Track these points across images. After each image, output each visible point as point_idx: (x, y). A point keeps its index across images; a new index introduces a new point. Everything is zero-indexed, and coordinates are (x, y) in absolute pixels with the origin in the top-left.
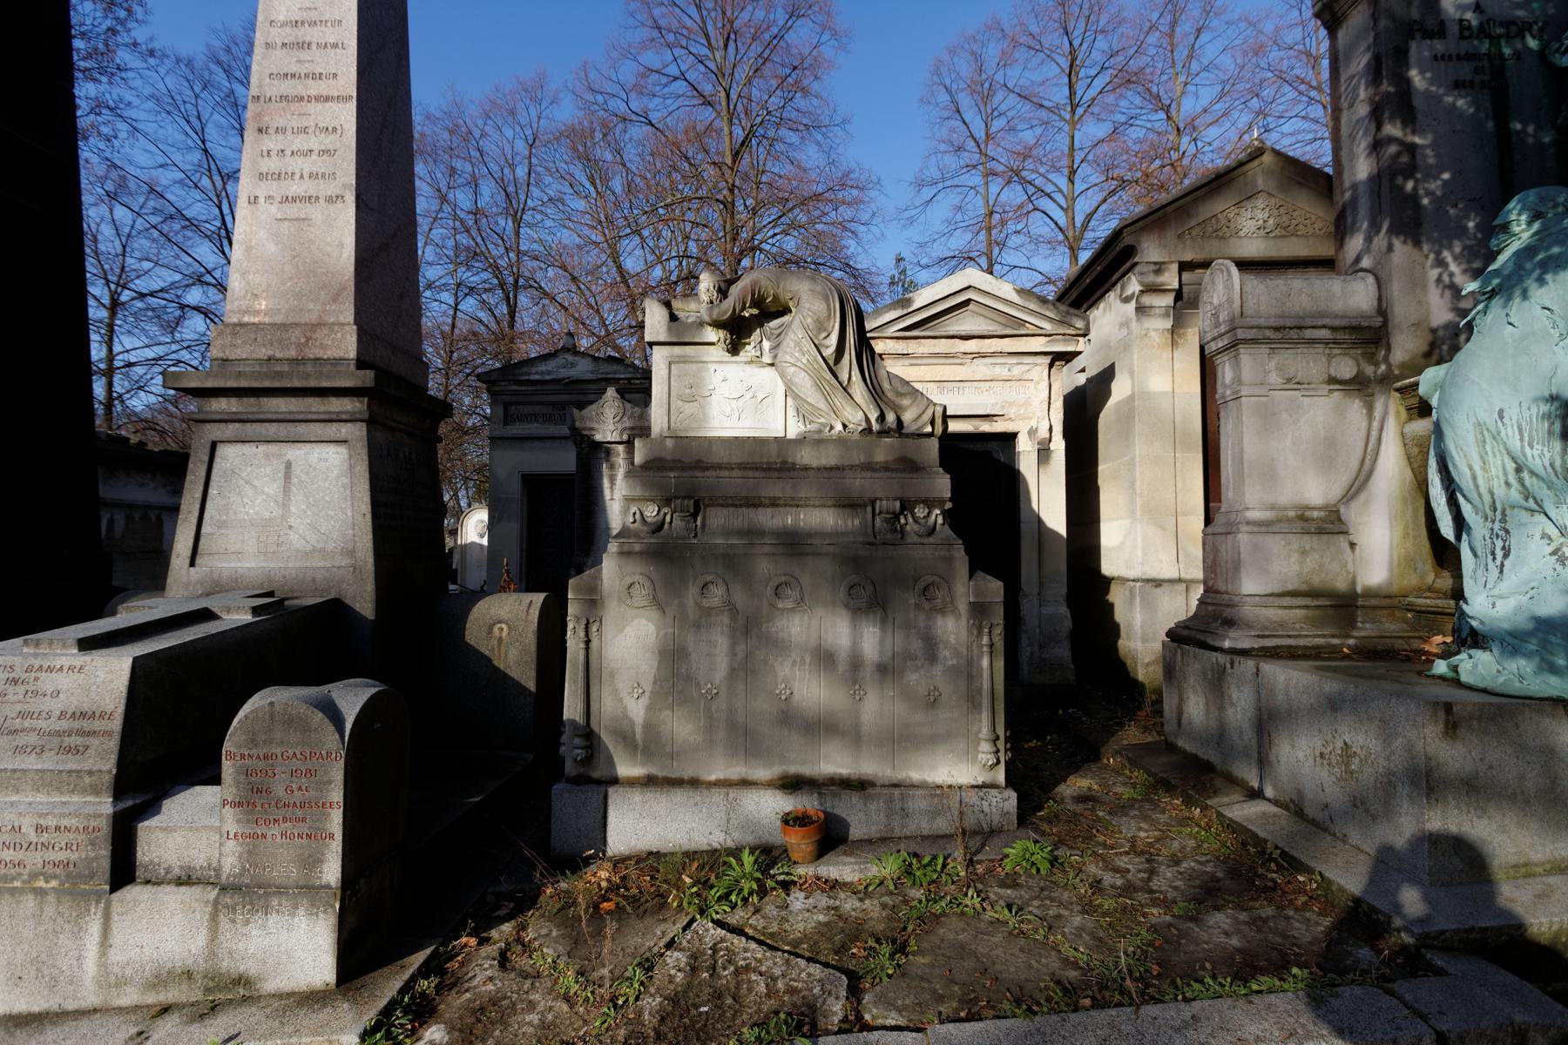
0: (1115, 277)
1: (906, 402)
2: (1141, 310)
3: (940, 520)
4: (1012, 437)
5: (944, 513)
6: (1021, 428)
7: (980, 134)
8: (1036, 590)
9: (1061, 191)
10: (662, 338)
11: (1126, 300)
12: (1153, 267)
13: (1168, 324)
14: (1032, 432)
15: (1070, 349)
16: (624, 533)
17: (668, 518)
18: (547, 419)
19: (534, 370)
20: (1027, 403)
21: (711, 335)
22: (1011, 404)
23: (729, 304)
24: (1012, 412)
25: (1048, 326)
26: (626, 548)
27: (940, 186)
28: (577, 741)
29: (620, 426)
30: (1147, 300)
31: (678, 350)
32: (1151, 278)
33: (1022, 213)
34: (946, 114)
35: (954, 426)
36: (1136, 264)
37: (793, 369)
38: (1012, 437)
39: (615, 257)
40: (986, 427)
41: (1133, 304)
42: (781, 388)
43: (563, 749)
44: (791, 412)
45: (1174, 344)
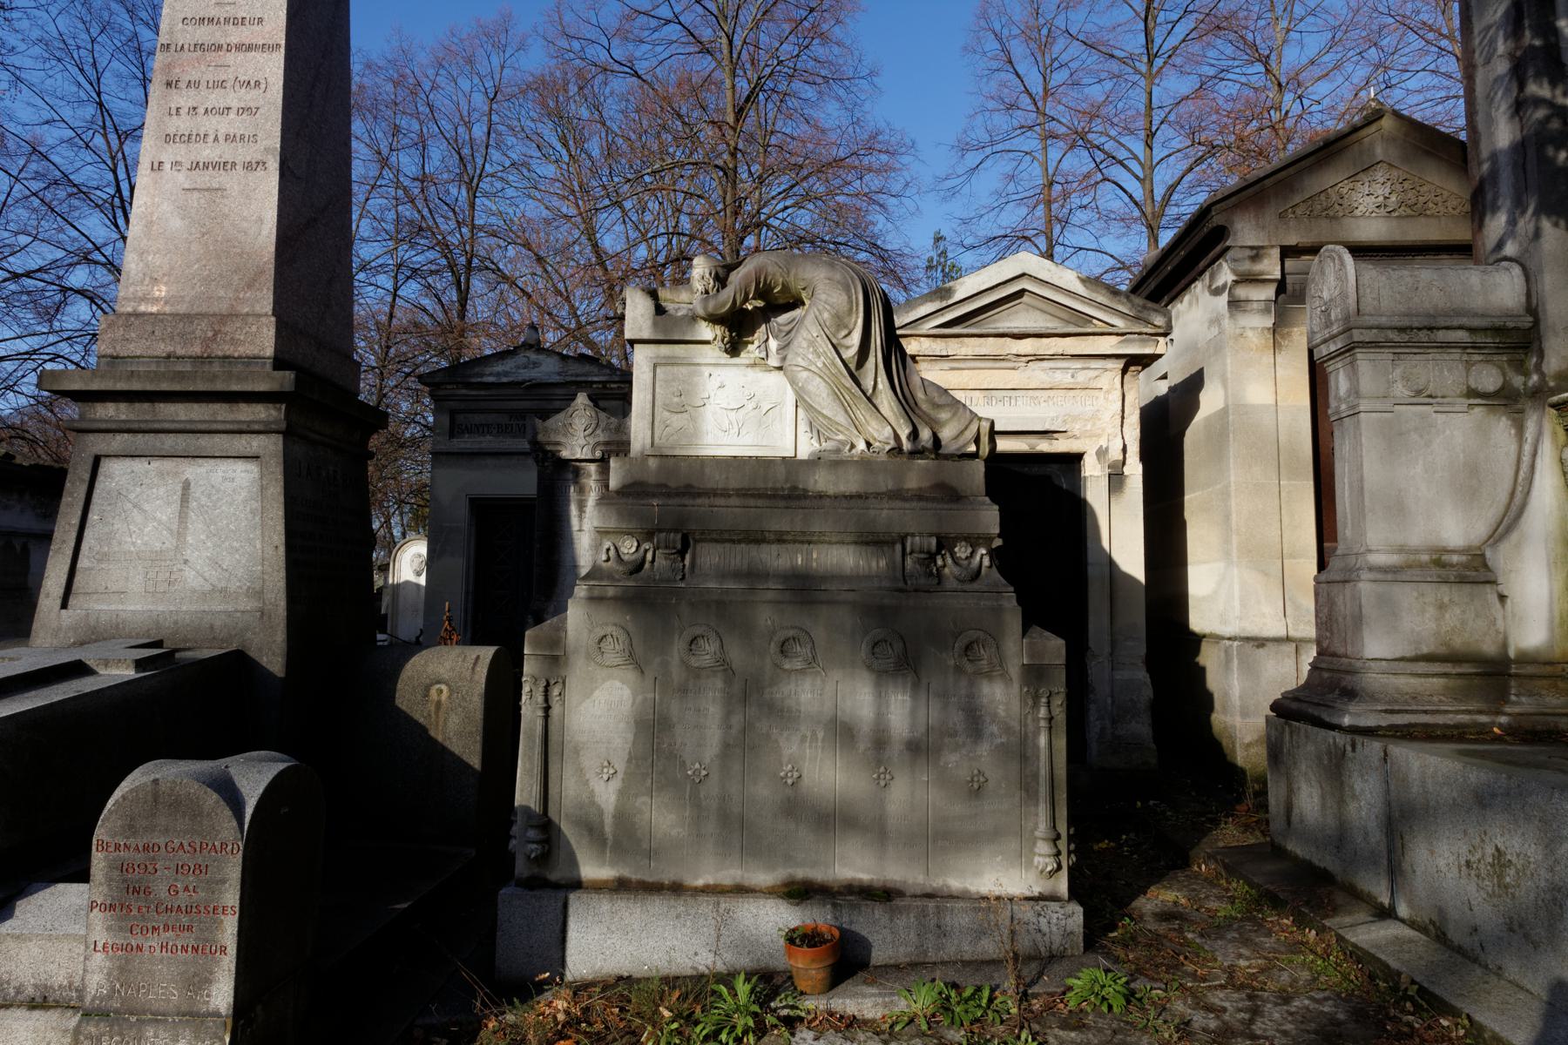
0: (1202, 264)
1: (944, 415)
2: (1235, 304)
3: (986, 562)
4: (1075, 459)
5: (992, 553)
6: (1089, 448)
7: (1037, 88)
8: (1107, 650)
9: (1136, 157)
10: (646, 335)
11: (1217, 292)
12: (1248, 253)
13: (1269, 322)
14: (1102, 453)
15: (1148, 351)
16: (595, 573)
17: (649, 556)
18: (502, 430)
19: (488, 370)
20: (1095, 417)
21: (706, 331)
22: (1075, 419)
23: (727, 294)
24: (1076, 428)
25: (1120, 323)
26: (596, 593)
27: (988, 150)
28: (532, 834)
29: (592, 441)
30: (1242, 292)
31: (665, 350)
32: (1246, 266)
33: (1088, 183)
34: (995, 65)
35: (1003, 445)
36: (1228, 248)
37: (805, 374)
38: (1075, 459)
39: (591, 233)
40: (1044, 446)
41: (1225, 297)
42: (791, 397)
43: (513, 842)
44: (803, 427)
45: (1276, 346)
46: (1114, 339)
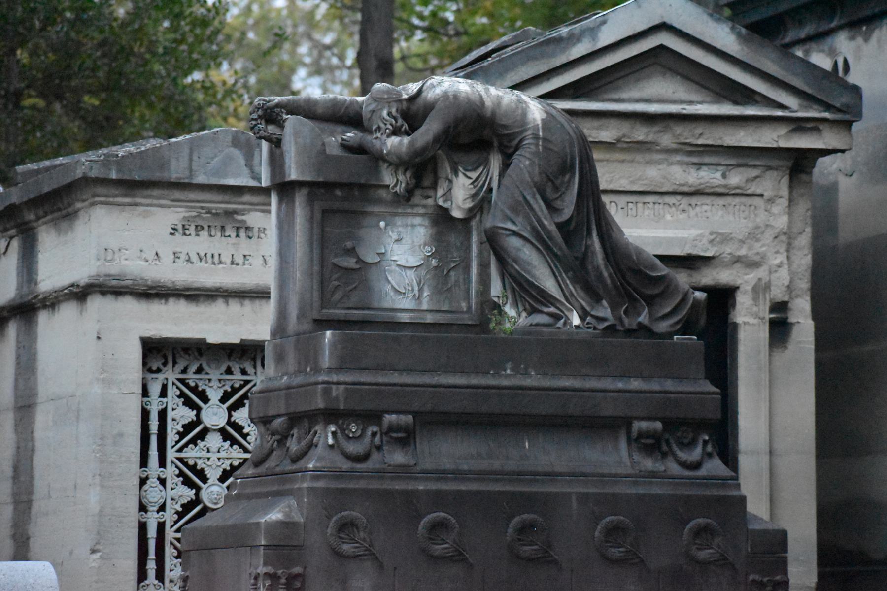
6: (744, 280)
46: (783, 130)
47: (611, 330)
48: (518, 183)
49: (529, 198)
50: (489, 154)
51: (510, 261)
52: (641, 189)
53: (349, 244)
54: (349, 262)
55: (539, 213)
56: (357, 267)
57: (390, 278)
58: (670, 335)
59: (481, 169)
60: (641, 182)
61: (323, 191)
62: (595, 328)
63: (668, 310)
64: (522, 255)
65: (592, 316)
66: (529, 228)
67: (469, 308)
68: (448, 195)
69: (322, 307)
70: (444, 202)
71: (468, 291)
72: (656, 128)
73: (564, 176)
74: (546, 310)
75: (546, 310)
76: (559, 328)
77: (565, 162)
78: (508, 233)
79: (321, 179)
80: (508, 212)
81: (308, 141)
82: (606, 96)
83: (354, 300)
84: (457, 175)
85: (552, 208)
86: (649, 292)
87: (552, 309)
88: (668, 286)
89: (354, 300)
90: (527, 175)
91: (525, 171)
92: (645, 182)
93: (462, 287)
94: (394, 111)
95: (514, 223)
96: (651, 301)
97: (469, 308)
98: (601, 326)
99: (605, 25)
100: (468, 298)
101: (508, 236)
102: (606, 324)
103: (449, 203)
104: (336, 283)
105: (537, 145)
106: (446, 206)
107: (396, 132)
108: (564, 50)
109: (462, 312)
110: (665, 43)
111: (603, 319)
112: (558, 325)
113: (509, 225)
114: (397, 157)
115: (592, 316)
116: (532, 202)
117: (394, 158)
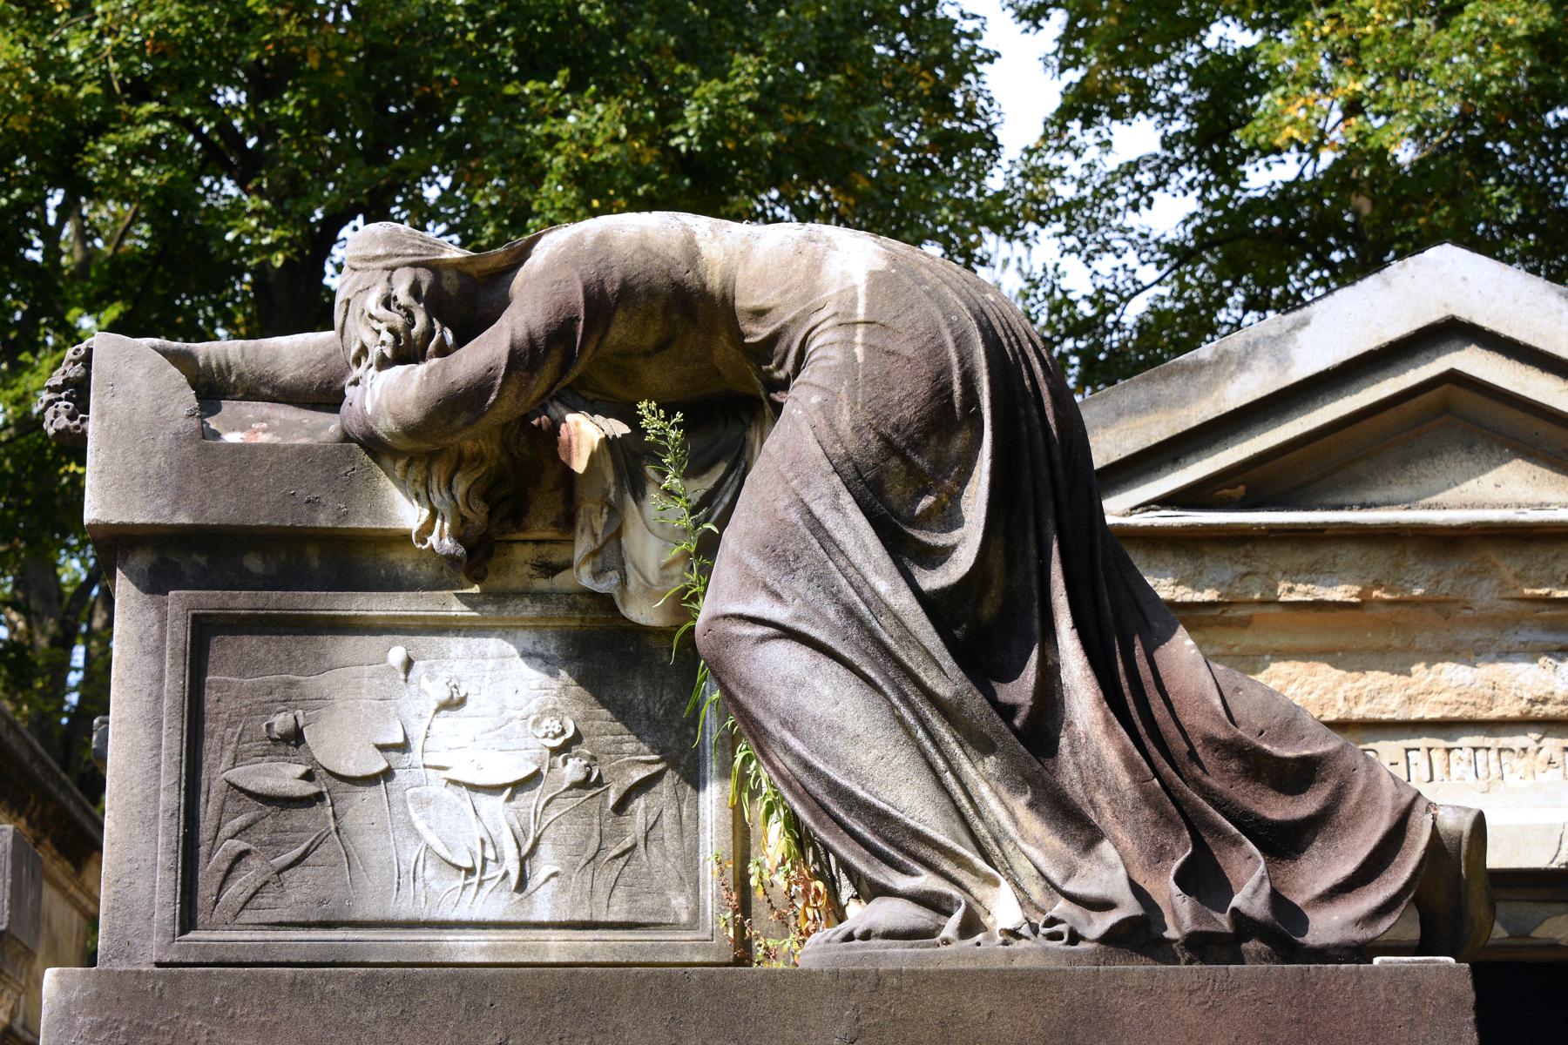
47: (1138, 936)
48: (783, 468)
49: (819, 509)
50: (747, 427)
51: (772, 725)
52: (1436, 714)
53: (281, 722)
54: (285, 777)
55: (857, 558)
56: (310, 789)
57: (420, 825)
58: (1361, 952)
59: (720, 470)
60: (1435, 698)
61: (202, 560)
62: (1075, 938)
63: (1345, 867)
64: (805, 700)
65: (1071, 897)
66: (831, 612)
67: (696, 914)
68: (611, 553)
69: (187, 920)
70: (597, 575)
71: (691, 858)
72: (1456, 566)
73: (946, 439)
74: (902, 883)
75: (902, 883)
76: (947, 942)
77: (941, 390)
78: (760, 631)
79: (183, 519)
80: (756, 564)
81: (144, 406)
82: (1329, 500)
83: (299, 893)
84: (639, 493)
85: (906, 551)
86: (1280, 809)
87: (925, 881)
88: (1338, 796)
89: (299, 893)
90: (810, 438)
91: (805, 428)
92: (1443, 697)
93: (671, 845)
94: (402, 292)
95: (777, 596)
96: (1284, 843)
97: (696, 914)
98: (1102, 923)
99: (1307, 329)
100: (690, 878)
101: (763, 639)
102: (1112, 918)
103: (613, 576)
104: (240, 845)
105: (849, 343)
106: (602, 587)
107: (406, 352)
108: (1209, 387)
109: (674, 926)
110: (1459, 367)
111: (1104, 905)
112: (944, 934)
113: (761, 606)
114: (394, 416)
115: (1071, 897)
116: (830, 521)
117: (390, 421)
